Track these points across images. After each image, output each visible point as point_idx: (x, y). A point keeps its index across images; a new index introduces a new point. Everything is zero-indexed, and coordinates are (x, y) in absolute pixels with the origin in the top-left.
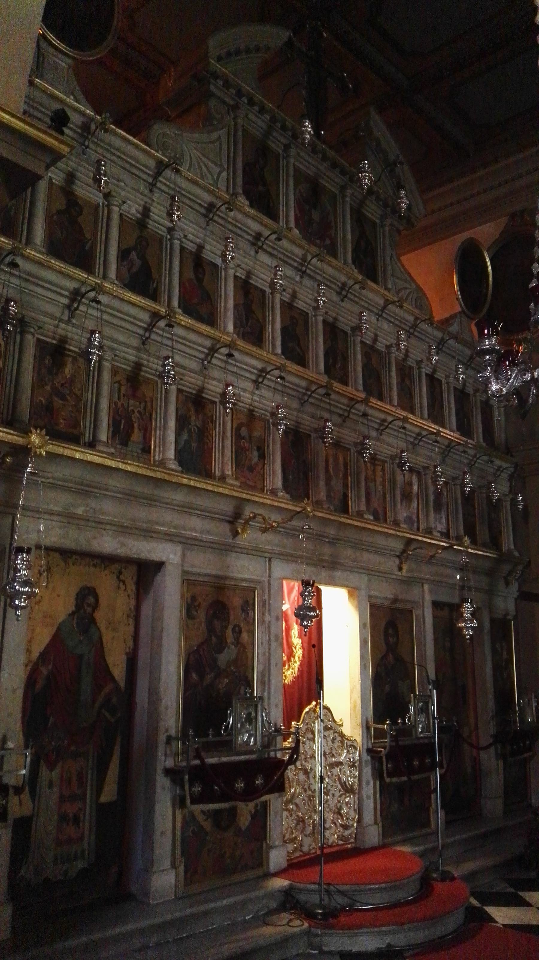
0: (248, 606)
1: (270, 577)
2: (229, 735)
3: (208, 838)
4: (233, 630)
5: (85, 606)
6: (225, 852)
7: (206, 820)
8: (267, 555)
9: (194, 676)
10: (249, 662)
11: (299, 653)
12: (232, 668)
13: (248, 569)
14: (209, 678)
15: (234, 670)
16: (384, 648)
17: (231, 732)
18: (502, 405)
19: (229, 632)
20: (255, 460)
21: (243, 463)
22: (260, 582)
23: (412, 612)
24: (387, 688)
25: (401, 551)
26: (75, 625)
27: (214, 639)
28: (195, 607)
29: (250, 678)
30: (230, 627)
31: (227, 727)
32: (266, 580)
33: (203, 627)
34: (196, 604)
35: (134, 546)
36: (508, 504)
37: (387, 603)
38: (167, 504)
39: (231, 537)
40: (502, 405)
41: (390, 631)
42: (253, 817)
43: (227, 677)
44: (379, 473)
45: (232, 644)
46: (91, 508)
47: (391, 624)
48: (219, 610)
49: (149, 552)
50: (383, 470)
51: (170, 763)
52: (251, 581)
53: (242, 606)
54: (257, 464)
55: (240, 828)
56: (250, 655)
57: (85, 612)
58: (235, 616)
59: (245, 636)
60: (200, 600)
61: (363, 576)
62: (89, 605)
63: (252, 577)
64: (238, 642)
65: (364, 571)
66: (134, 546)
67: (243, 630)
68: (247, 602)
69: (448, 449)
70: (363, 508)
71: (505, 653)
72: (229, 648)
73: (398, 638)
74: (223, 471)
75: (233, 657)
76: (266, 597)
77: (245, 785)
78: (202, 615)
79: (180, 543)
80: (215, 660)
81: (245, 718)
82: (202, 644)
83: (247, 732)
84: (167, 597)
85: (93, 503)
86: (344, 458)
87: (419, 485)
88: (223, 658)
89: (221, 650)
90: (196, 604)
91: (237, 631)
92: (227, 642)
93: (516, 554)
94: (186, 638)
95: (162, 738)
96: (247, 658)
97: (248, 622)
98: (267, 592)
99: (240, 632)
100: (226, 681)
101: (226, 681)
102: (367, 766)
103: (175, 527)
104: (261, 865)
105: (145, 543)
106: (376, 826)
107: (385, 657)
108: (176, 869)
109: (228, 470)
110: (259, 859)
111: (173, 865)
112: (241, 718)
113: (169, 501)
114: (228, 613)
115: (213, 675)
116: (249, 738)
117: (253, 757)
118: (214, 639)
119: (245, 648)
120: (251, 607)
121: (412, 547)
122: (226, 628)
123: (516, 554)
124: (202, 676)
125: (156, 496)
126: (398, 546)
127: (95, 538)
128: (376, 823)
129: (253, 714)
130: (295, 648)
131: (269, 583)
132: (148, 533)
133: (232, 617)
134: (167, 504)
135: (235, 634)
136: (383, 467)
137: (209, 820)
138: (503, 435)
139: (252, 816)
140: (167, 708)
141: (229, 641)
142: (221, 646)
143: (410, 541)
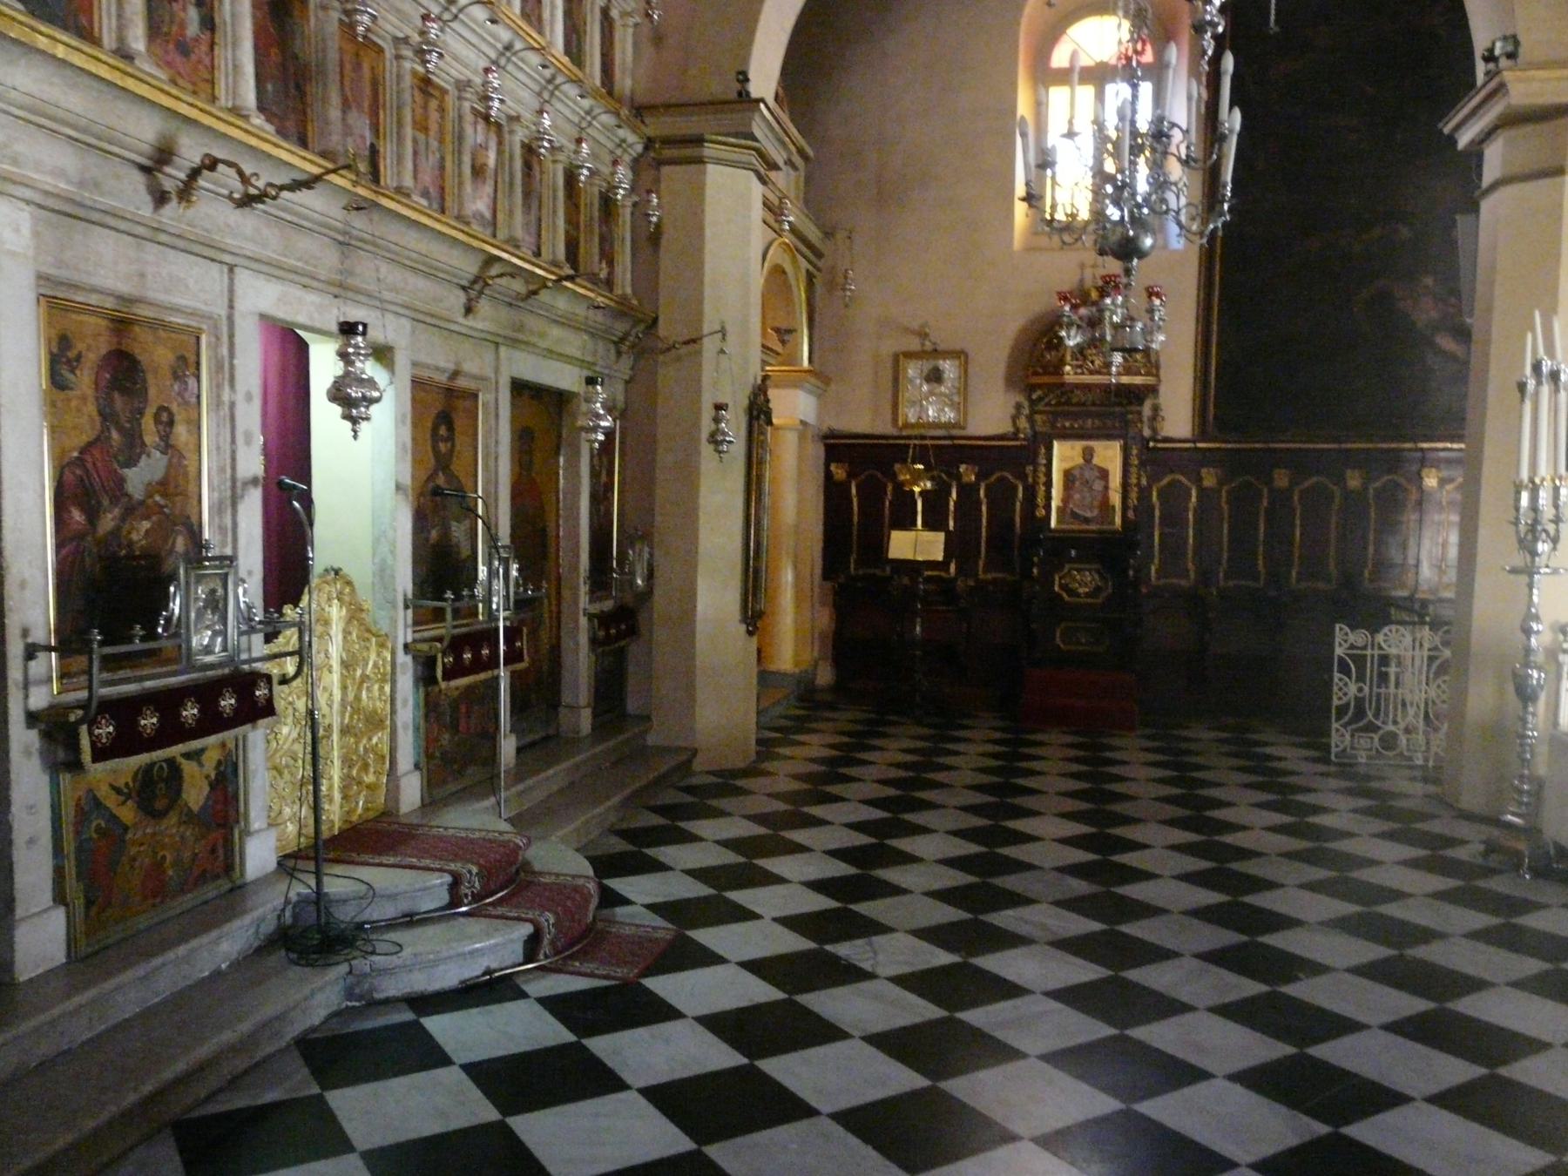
0: (186, 366)
1: (231, 307)
2: (176, 635)
3: (129, 836)
4: (157, 420)
6: (164, 857)
7: (124, 803)
8: (228, 258)
9: (77, 516)
10: (192, 488)
12: (157, 498)
13: (187, 286)
14: (108, 522)
15: (162, 502)
16: (431, 462)
17: (179, 630)
18: (631, 21)
19: (148, 423)
20: (193, 29)
21: (165, 29)
22: (210, 318)
23: (476, 396)
24: (434, 534)
25: (471, 277)
27: (115, 435)
28: (69, 362)
29: (194, 519)
30: (150, 411)
31: (168, 620)
32: (223, 312)
33: (91, 408)
34: (72, 354)
36: (628, 211)
37: (442, 378)
39: (151, 206)
40: (631, 21)
41: (443, 431)
42: (213, 786)
43: (147, 518)
44: (434, 116)
47: (445, 419)
48: (124, 371)
50: (442, 109)
51: (39, 699)
52: (193, 314)
53: (172, 367)
54: (197, 40)
55: (190, 810)
56: (192, 470)
58: (158, 389)
59: (181, 432)
60: (80, 346)
61: (404, 321)
64: (167, 446)
65: (407, 312)
67: (177, 418)
68: (182, 359)
69: (551, 87)
70: (408, 182)
71: (604, 473)
72: (149, 456)
73: (453, 446)
74: (121, 39)
75: (159, 474)
76: (225, 351)
77: (115, 729)
78: (84, 380)
79: (28, 202)
80: (121, 481)
81: (205, 601)
82: (90, 445)
83: (208, 627)
84: (695, 118)
86: (373, 68)
87: (500, 152)
88: (138, 478)
89: (132, 462)
90: (72, 354)
91: (166, 422)
92: (143, 444)
93: (635, 302)
94: (53, 430)
95: (15, 649)
96: (186, 474)
97: (187, 403)
98: (225, 339)
99: (171, 423)
100: (146, 525)
101: (146, 525)
102: (404, 673)
104: (228, 868)
106: (417, 773)
107: (431, 478)
108: (66, 905)
109: (136, 39)
110: (225, 859)
111: (60, 898)
112: (197, 599)
114: (144, 381)
115: (117, 511)
116: (212, 638)
117: (227, 671)
119: (182, 457)
120: (192, 369)
121: (494, 271)
122: (141, 413)
123: (635, 302)
124: (93, 515)
126: (469, 267)
129: (220, 592)
131: (230, 319)
133: (152, 392)
135: (161, 428)
136: (442, 101)
137: (129, 803)
138: (628, 83)
139: (211, 785)
140: (23, 585)
141: (148, 439)
142: (133, 450)
143: (491, 260)
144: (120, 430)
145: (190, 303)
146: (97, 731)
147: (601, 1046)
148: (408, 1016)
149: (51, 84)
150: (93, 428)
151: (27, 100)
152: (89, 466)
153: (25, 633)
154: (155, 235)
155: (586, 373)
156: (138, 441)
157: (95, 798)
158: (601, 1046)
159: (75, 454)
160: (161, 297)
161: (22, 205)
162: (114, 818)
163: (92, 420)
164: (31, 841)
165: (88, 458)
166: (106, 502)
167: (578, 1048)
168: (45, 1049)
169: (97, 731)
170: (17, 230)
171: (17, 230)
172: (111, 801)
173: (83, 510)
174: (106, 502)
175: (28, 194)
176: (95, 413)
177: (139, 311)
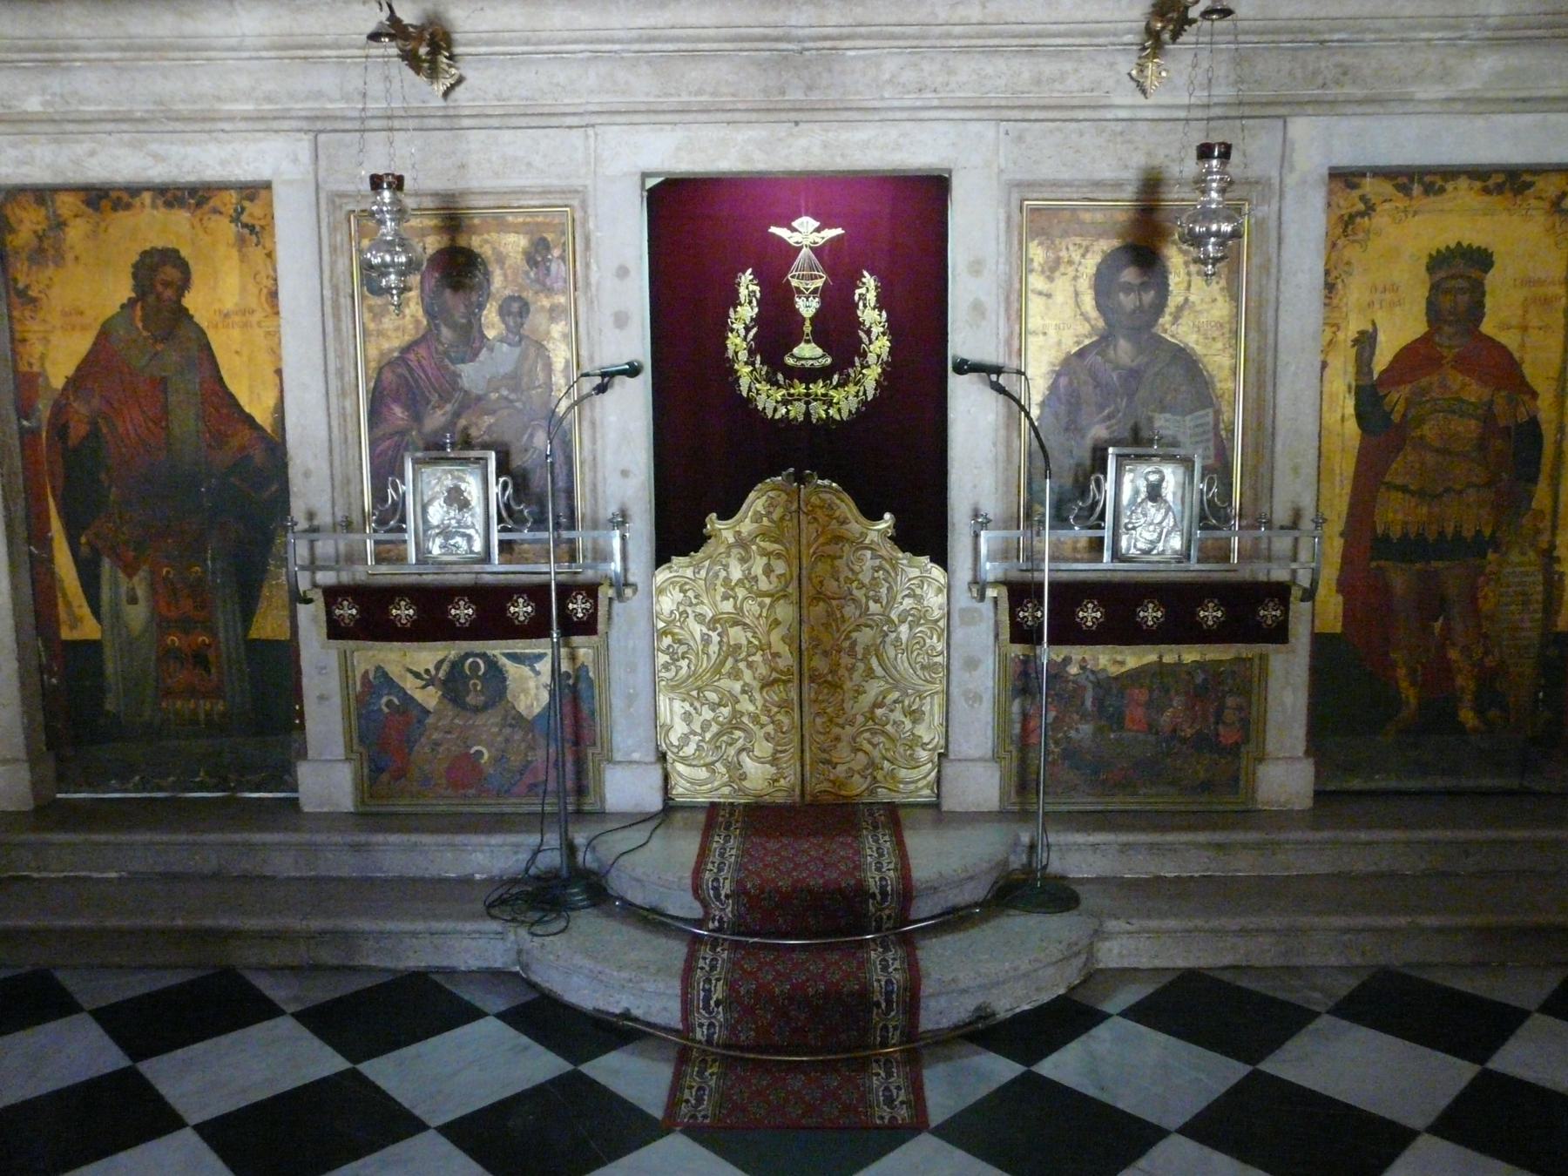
3: (430, 720)
5: (160, 288)
11: (879, 347)
13: (529, 164)
22: (577, 192)
26: (140, 325)
27: (446, 333)
35: (185, 157)
38: (233, 49)
45: (502, 341)
46: (54, 94)
48: (458, 267)
49: (223, 163)
52: (545, 192)
57: (159, 297)
62: (166, 284)
63: (547, 181)
66: (185, 157)
75: (507, 368)
77: (389, 613)
85: (55, 83)
103: (268, 99)
105: (213, 148)
113: (233, 41)
118: (446, 333)
125: (138, 37)
127: (92, 154)
128: (996, 758)
130: (868, 332)
132: (205, 121)
134: (233, 49)
141: (491, 334)
144: (453, 326)
145: (539, 182)
146: (338, 612)
147: (384, 1071)
148: (1001, 1069)
149: (279, 17)
150: (417, 328)
151: (265, 41)
152: (413, 364)
153: (311, 516)
154: (451, 122)
155: (1198, 138)
156: (475, 333)
157: (385, 675)
158: (384, 1071)
159: (396, 354)
160: (489, 184)
161: (299, 135)
162: (407, 699)
163: (417, 322)
164: (322, 698)
165: (412, 356)
166: (435, 398)
167: (356, 1060)
168: (246, 865)
169: (338, 612)
170: (295, 160)
171: (295, 160)
172: (410, 685)
173: (406, 407)
174: (435, 398)
175: (294, 124)
176: (420, 313)
177: (475, 203)
